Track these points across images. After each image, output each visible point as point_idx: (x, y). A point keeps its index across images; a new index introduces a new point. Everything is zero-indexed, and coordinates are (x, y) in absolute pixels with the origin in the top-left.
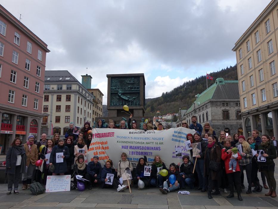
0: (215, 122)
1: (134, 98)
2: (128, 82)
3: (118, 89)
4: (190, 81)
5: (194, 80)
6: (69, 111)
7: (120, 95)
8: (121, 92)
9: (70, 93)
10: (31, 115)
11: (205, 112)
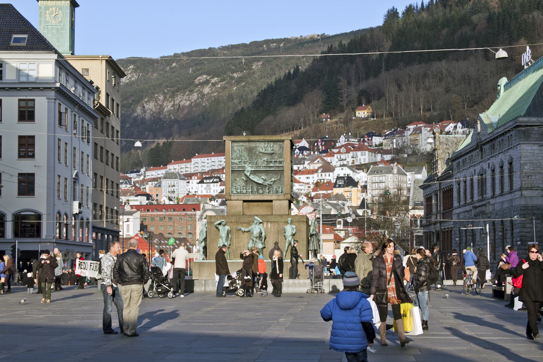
0: (531, 197)
1: (273, 179)
2: (263, 151)
3: (245, 163)
6: (30, 157)
7: (248, 174)
8: (250, 169)
11: (504, 158)
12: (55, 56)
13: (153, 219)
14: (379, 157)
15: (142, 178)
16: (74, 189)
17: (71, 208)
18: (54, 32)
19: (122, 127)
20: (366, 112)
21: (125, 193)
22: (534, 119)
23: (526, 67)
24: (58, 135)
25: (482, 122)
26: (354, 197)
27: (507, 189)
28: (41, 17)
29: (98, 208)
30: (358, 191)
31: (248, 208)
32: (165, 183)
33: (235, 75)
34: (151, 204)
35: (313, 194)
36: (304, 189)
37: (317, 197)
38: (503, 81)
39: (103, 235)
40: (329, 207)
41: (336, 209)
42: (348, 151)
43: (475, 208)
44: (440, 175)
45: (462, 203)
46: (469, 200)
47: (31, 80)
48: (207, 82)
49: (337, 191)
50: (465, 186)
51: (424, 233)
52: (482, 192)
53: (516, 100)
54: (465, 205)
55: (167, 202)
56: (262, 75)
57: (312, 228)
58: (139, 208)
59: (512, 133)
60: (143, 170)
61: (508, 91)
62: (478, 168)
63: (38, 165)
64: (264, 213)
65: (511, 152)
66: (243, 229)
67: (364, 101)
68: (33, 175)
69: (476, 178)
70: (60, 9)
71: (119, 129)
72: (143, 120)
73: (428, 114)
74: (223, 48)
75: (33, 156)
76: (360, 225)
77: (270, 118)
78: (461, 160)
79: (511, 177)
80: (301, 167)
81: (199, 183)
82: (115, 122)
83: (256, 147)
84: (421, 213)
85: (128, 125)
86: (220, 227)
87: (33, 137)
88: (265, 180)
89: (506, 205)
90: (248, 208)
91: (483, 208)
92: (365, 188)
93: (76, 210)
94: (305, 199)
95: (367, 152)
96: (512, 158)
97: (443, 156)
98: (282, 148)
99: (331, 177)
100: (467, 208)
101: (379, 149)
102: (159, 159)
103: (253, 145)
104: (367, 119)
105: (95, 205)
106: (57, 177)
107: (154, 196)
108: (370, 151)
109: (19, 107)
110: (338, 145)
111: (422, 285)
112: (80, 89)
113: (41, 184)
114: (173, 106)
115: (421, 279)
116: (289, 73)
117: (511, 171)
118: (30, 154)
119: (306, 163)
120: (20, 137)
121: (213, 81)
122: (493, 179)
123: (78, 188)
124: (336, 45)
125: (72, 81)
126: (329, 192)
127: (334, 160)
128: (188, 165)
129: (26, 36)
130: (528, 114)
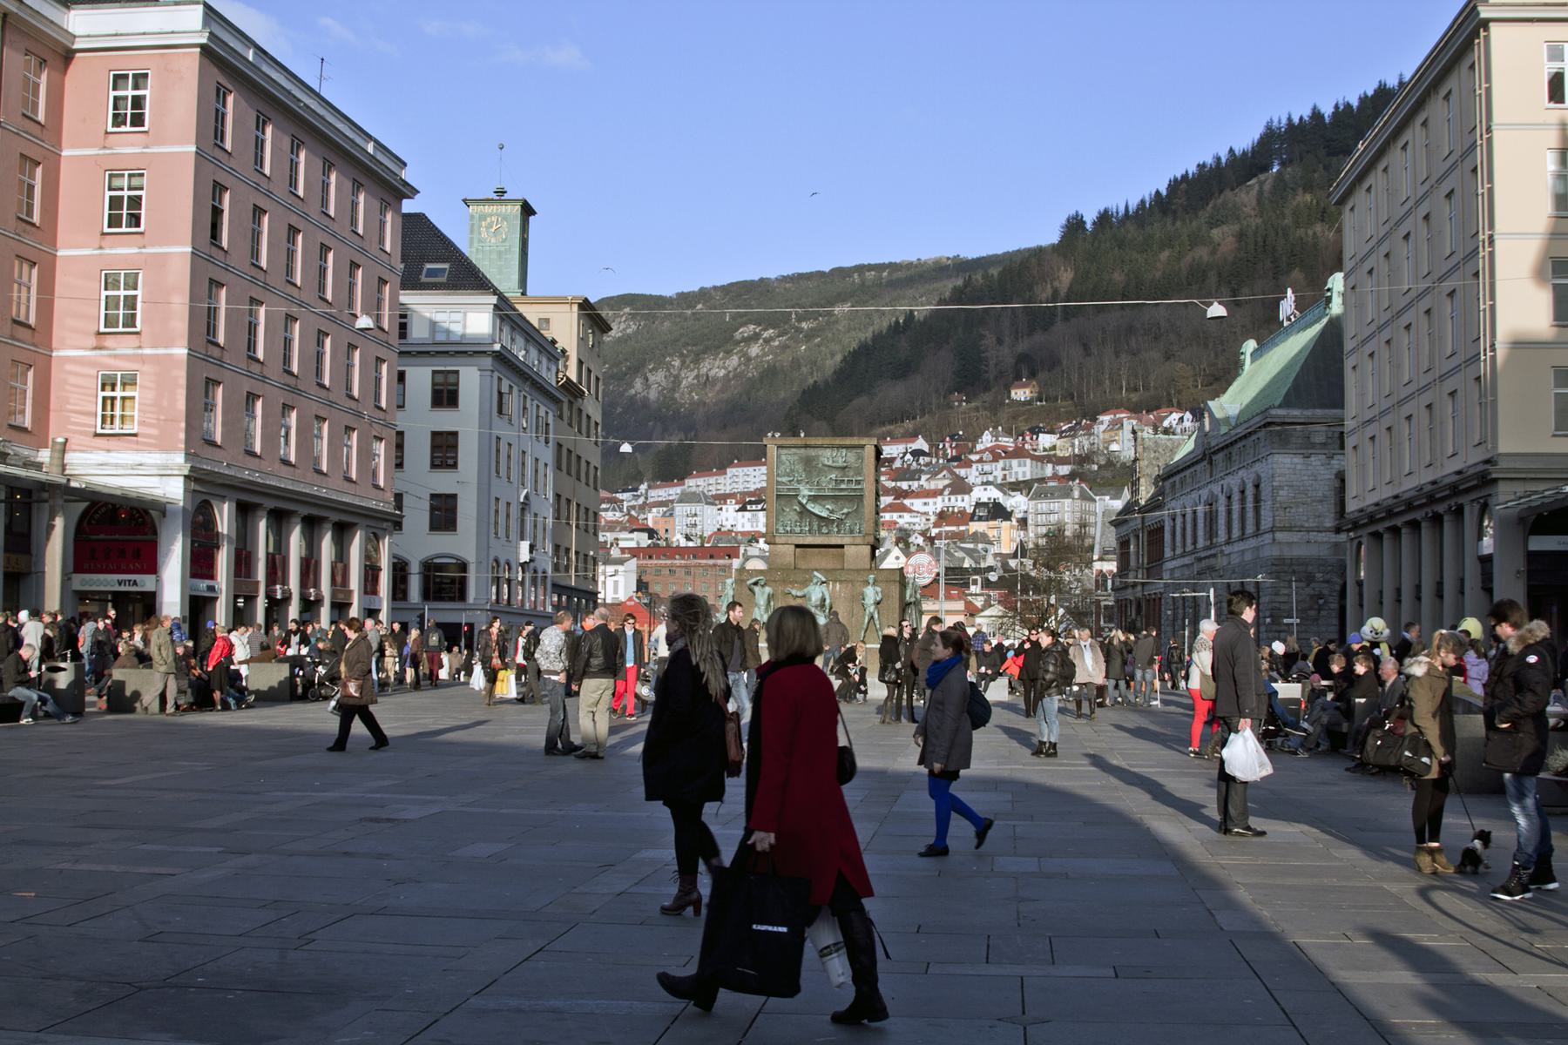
0: (1290, 544)
3: (799, 482)
4: (1316, 115)
5: (1355, 103)
8: (807, 493)
9: (453, 360)
10: (366, 516)
11: (1247, 476)
12: (494, 299)
13: (658, 571)
14: (1049, 470)
15: (641, 501)
16: (523, 521)
17: (517, 554)
18: (494, 256)
19: (604, 414)
20: (1028, 391)
21: (612, 526)
22: (1296, 412)
23: (1286, 324)
24: (496, 432)
25: (1211, 415)
26: (1005, 537)
27: (1250, 529)
28: (472, 232)
29: (562, 552)
30: (1012, 527)
31: (804, 557)
32: (680, 509)
33: (804, 325)
34: (656, 546)
35: (934, 532)
36: (920, 523)
37: (939, 536)
38: (1250, 345)
39: (569, 598)
40: (960, 554)
41: (972, 557)
42: (996, 458)
43: (1200, 560)
44: (1142, 502)
45: (1179, 551)
46: (1189, 548)
47: (453, 339)
48: (755, 337)
49: (975, 527)
50: (1184, 522)
51: (1117, 601)
52: (1211, 533)
53: (1268, 378)
54: (1182, 556)
55: (683, 543)
56: (854, 323)
57: (908, 593)
58: (635, 552)
59: (1259, 435)
60: (643, 487)
61: (1261, 360)
62: (1204, 493)
63: (464, 481)
64: (830, 566)
65: (1257, 467)
66: (794, 592)
67: (1025, 372)
68: (454, 497)
69: (1200, 509)
70: (505, 218)
71: (599, 420)
72: (645, 402)
73: (1134, 397)
74: (785, 279)
75: (455, 466)
76: (1009, 585)
77: (862, 400)
78: (1177, 478)
79: (1257, 510)
80: (915, 485)
81: (740, 510)
82: (592, 408)
83: (818, 457)
84: (1111, 566)
85: (619, 410)
86: (757, 589)
87: (455, 434)
88: (832, 512)
89: (1248, 557)
90: (804, 557)
91: (1212, 561)
92: (1023, 523)
93: (525, 556)
94: (920, 540)
95: (1028, 461)
96: (1259, 477)
97: (1148, 471)
98: (860, 458)
99: (965, 503)
100: (1187, 560)
101: (1051, 458)
102: (672, 468)
103: (812, 452)
104: (1028, 403)
105: (557, 548)
106: (493, 501)
107: (662, 533)
108: (1033, 458)
109: (434, 384)
110: (979, 447)
111: (1049, 687)
112: (534, 353)
113: (467, 511)
114: (697, 377)
115: (1048, 677)
116: (897, 322)
117: (1257, 499)
118: (450, 462)
119: (924, 477)
120: (435, 434)
121: (766, 335)
122: (1229, 512)
123: (529, 519)
124: (978, 277)
125: (520, 341)
126: (962, 528)
127: (972, 475)
128: (721, 479)
129: (446, 266)
130: (1287, 403)
